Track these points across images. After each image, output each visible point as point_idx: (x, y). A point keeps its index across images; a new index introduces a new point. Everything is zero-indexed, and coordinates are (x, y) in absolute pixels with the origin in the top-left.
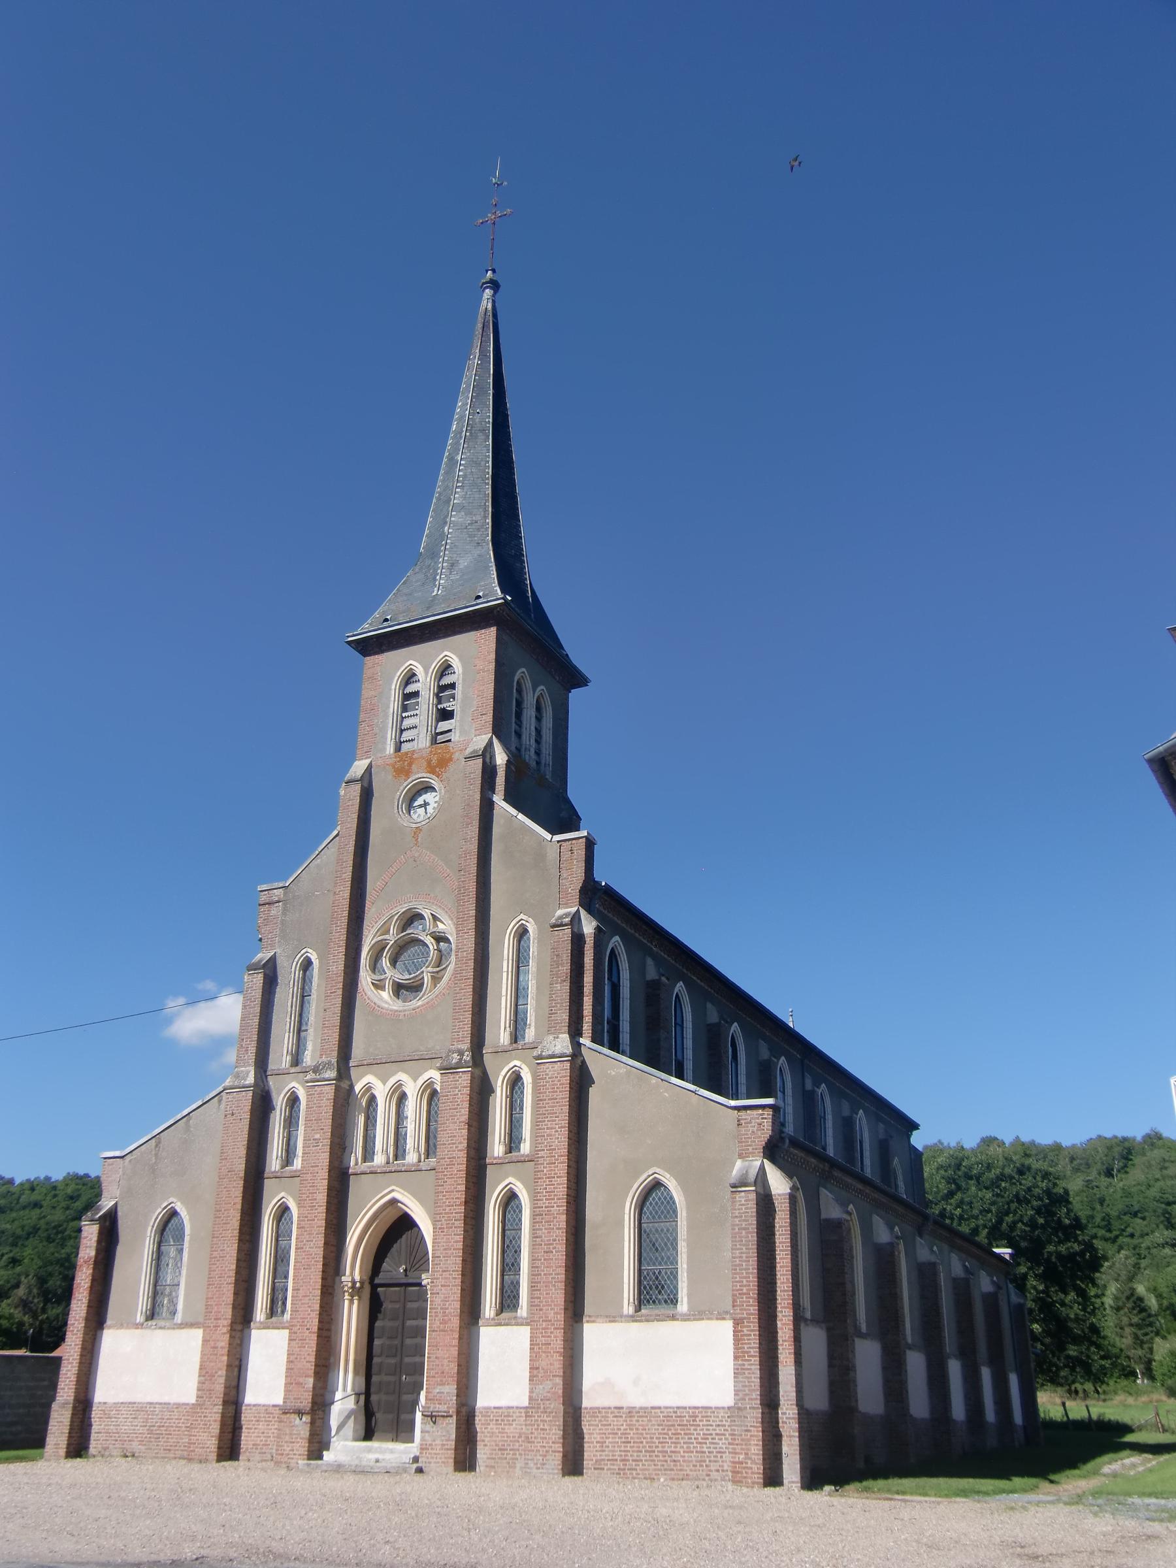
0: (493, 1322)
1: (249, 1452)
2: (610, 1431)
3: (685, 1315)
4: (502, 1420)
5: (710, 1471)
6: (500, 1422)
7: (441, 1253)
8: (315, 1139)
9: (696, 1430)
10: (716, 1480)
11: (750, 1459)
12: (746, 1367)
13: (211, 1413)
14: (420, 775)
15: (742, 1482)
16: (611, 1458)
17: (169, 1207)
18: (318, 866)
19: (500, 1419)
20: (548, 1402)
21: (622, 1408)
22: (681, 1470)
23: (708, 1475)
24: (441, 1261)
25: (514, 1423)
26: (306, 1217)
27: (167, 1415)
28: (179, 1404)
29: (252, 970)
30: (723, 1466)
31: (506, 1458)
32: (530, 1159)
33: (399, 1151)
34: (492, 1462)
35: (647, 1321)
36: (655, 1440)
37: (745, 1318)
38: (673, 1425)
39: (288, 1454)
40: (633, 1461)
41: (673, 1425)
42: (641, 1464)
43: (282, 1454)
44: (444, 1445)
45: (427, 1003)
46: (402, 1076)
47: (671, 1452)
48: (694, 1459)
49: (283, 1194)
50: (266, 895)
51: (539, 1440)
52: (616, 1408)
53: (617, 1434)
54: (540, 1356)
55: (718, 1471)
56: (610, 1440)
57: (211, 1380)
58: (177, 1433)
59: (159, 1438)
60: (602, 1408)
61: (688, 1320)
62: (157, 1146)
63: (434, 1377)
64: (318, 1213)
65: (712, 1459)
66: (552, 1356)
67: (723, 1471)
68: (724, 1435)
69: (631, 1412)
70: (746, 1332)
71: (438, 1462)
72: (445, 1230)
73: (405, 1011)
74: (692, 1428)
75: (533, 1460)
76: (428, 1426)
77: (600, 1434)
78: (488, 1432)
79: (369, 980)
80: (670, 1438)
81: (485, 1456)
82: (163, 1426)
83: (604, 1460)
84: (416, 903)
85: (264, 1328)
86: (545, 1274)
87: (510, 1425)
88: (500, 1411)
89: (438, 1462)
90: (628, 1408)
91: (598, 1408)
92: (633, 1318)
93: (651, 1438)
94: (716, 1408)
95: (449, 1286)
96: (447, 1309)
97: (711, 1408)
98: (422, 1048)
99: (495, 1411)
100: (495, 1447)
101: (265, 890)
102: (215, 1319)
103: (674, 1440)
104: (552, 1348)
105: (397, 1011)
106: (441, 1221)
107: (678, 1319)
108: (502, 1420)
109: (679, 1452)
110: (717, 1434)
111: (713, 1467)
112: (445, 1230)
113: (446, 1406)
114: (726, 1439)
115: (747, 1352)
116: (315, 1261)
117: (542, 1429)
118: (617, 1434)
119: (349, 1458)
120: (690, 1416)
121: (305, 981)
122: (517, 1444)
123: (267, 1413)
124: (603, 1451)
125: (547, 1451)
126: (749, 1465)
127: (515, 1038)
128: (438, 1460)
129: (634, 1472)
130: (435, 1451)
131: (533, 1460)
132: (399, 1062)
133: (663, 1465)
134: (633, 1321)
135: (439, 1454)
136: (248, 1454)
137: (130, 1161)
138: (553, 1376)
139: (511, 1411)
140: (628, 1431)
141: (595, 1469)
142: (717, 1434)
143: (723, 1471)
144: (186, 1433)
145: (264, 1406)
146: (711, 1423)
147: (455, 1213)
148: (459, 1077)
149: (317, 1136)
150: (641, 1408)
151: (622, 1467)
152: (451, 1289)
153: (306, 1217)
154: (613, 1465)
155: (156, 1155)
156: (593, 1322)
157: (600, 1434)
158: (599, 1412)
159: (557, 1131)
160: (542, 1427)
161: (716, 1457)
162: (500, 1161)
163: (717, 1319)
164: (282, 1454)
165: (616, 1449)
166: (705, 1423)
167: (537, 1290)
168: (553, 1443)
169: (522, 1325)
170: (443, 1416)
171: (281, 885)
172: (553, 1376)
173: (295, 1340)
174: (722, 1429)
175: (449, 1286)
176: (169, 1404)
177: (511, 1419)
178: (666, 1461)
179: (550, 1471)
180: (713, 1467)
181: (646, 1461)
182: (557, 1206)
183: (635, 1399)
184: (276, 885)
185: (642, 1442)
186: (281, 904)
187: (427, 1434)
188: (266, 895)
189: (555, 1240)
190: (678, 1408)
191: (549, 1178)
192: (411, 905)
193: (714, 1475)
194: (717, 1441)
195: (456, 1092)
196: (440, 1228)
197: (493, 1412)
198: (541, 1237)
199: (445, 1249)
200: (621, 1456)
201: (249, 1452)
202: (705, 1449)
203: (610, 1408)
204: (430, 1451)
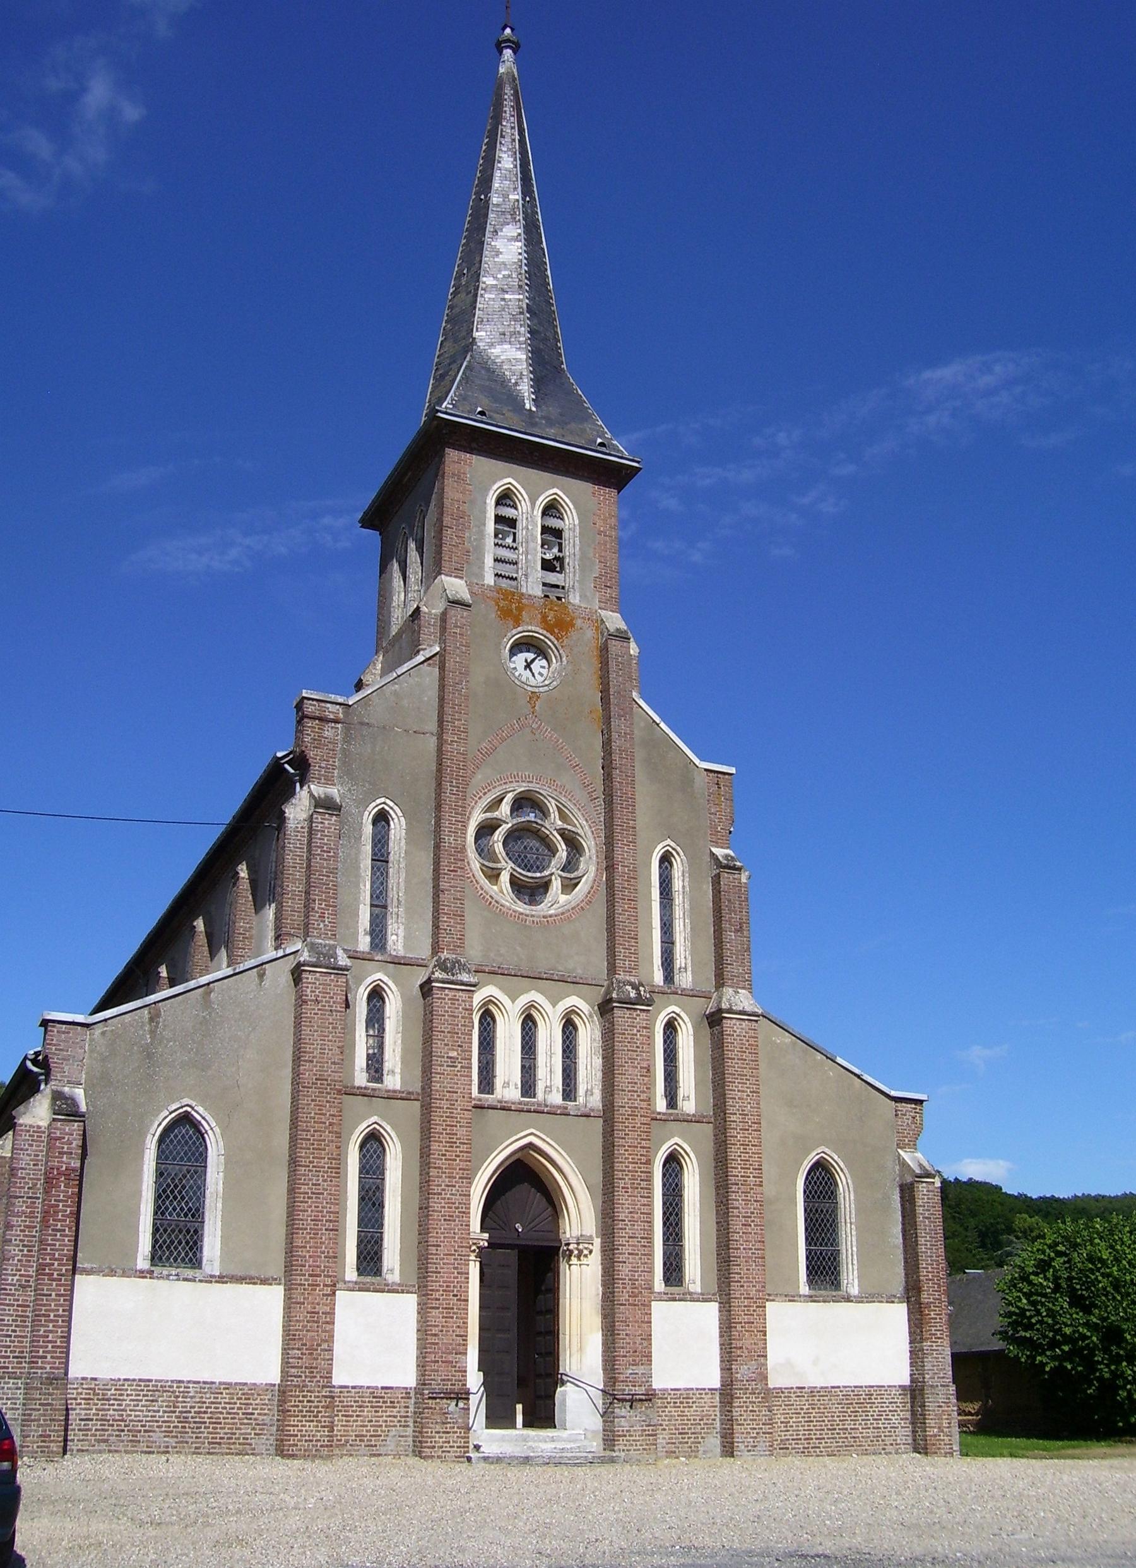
0: (665, 1297)
1: (351, 1445)
2: (793, 1411)
3: (858, 1297)
4: (681, 1403)
5: (886, 1445)
6: (678, 1404)
7: (627, 1217)
8: (451, 1058)
9: (871, 1407)
10: (890, 1453)
11: (943, 1431)
12: (934, 1348)
13: (318, 1397)
14: (533, 628)
15: (936, 1453)
16: (795, 1437)
17: (181, 1111)
18: (395, 693)
19: (678, 1401)
20: (754, 1383)
21: (804, 1388)
22: (860, 1446)
23: (884, 1449)
24: (627, 1225)
25: (694, 1405)
26: (443, 1155)
27: (209, 1398)
28: (230, 1384)
29: (322, 807)
30: (896, 1440)
31: (687, 1443)
32: (697, 1119)
33: (528, 1086)
34: (672, 1448)
35: (824, 1301)
36: (835, 1418)
37: (931, 1303)
38: (852, 1404)
39: (442, 1447)
40: (816, 1439)
41: (852, 1404)
42: (823, 1441)
43: (434, 1447)
44: (645, 1430)
45: (563, 914)
46: (534, 996)
47: (851, 1429)
48: (871, 1434)
49: (375, 1119)
50: (315, 705)
51: (749, 1422)
52: (798, 1388)
53: (800, 1413)
54: (744, 1335)
55: (892, 1444)
56: (794, 1420)
57: (311, 1354)
58: (230, 1421)
59: (201, 1428)
60: (785, 1388)
61: (862, 1302)
62: (151, 1019)
63: (626, 1356)
64: (461, 1152)
65: (887, 1434)
66: (756, 1336)
67: (897, 1444)
68: (896, 1411)
69: (813, 1391)
70: (933, 1316)
71: (639, 1450)
72: (630, 1190)
73: (533, 916)
74: (869, 1406)
75: (743, 1442)
76: (623, 1410)
77: (783, 1414)
78: (666, 1416)
79: (478, 865)
80: (850, 1416)
81: (664, 1441)
82: (205, 1412)
83: (788, 1440)
84: (538, 786)
85: (360, 1290)
86: (744, 1249)
87: (689, 1407)
88: (679, 1392)
89: (639, 1450)
90: (809, 1388)
91: (781, 1388)
92: (812, 1299)
93: (833, 1416)
94: (889, 1386)
95: (638, 1254)
96: (637, 1280)
97: (884, 1386)
98: (560, 968)
99: (673, 1392)
100: (674, 1431)
101: (313, 700)
102: (310, 1275)
103: (853, 1418)
104: (756, 1327)
105: (522, 914)
106: (624, 1179)
107: (852, 1301)
108: (681, 1403)
109: (858, 1429)
110: (890, 1411)
111: (888, 1441)
112: (630, 1190)
113: (643, 1388)
114: (898, 1415)
115: (934, 1334)
116: (459, 1212)
117: (751, 1411)
118: (800, 1413)
119: (518, 1449)
120: (866, 1395)
121: (380, 842)
122: (699, 1427)
123: (374, 1397)
124: (788, 1431)
125: (757, 1433)
126: (942, 1438)
127: (669, 977)
128: (638, 1447)
129: (818, 1450)
130: (634, 1438)
131: (743, 1442)
132: (535, 978)
133: (843, 1442)
134: (812, 1301)
135: (639, 1441)
136: (349, 1447)
137: (103, 1033)
138: (758, 1356)
139: (691, 1392)
140: (811, 1411)
141: (780, 1449)
142: (890, 1411)
143: (897, 1444)
144: (245, 1421)
145: (368, 1388)
146: (884, 1400)
147: (641, 1172)
148: (637, 1015)
149: (454, 1054)
150: (822, 1388)
151: (806, 1446)
152: (641, 1259)
153: (443, 1155)
154: (797, 1444)
155: (152, 1032)
156: (773, 1300)
157: (783, 1414)
158: (782, 1392)
159: (748, 1096)
160: (751, 1408)
161: (890, 1432)
162: (664, 1117)
163: (887, 1302)
164: (434, 1447)
165: (800, 1428)
166: (879, 1401)
167: (737, 1265)
168: (763, 1424)
169: (698, 1301)
170: (641, 1400)
171: (340, 700)
172: (758, 1356)
173: (438, 1308)
174: (894, 1405)
175: (638, 1254)
176: (213, 1383)
177: (691, 1401)
178: (846, 1438)
179: (762, 1453)
180: (888, 1441)
181: (828, 1438)
182: (754, 1177)
183: (816, 1379)
184: (333, 697)
185: (824, 1421)
186: (339, 726)
187: (623, 1419)
188: (315, 705)
189: (753, 1213)
190: (855, 1387)
191: (743, 1145)
192: (533, 786)
193: (889, 1448)
194: (890, 1417)
195: (635, 1032)
196: (623, 1188)
197: (670, 1394)
198: (738, 1208)
199: (631, 1213)
200: (805, 1435)
201: (351, 1445)
202: (880, 1425)
203: (792, 1388)
204: (628, 1438)
